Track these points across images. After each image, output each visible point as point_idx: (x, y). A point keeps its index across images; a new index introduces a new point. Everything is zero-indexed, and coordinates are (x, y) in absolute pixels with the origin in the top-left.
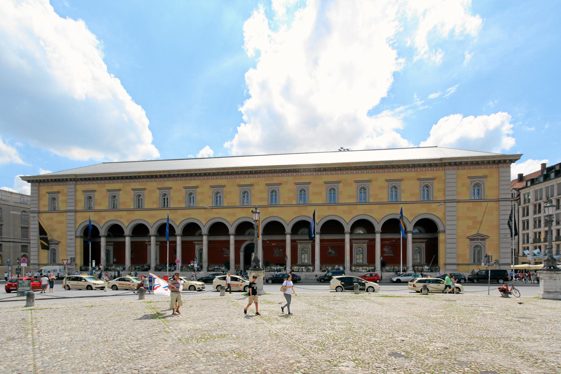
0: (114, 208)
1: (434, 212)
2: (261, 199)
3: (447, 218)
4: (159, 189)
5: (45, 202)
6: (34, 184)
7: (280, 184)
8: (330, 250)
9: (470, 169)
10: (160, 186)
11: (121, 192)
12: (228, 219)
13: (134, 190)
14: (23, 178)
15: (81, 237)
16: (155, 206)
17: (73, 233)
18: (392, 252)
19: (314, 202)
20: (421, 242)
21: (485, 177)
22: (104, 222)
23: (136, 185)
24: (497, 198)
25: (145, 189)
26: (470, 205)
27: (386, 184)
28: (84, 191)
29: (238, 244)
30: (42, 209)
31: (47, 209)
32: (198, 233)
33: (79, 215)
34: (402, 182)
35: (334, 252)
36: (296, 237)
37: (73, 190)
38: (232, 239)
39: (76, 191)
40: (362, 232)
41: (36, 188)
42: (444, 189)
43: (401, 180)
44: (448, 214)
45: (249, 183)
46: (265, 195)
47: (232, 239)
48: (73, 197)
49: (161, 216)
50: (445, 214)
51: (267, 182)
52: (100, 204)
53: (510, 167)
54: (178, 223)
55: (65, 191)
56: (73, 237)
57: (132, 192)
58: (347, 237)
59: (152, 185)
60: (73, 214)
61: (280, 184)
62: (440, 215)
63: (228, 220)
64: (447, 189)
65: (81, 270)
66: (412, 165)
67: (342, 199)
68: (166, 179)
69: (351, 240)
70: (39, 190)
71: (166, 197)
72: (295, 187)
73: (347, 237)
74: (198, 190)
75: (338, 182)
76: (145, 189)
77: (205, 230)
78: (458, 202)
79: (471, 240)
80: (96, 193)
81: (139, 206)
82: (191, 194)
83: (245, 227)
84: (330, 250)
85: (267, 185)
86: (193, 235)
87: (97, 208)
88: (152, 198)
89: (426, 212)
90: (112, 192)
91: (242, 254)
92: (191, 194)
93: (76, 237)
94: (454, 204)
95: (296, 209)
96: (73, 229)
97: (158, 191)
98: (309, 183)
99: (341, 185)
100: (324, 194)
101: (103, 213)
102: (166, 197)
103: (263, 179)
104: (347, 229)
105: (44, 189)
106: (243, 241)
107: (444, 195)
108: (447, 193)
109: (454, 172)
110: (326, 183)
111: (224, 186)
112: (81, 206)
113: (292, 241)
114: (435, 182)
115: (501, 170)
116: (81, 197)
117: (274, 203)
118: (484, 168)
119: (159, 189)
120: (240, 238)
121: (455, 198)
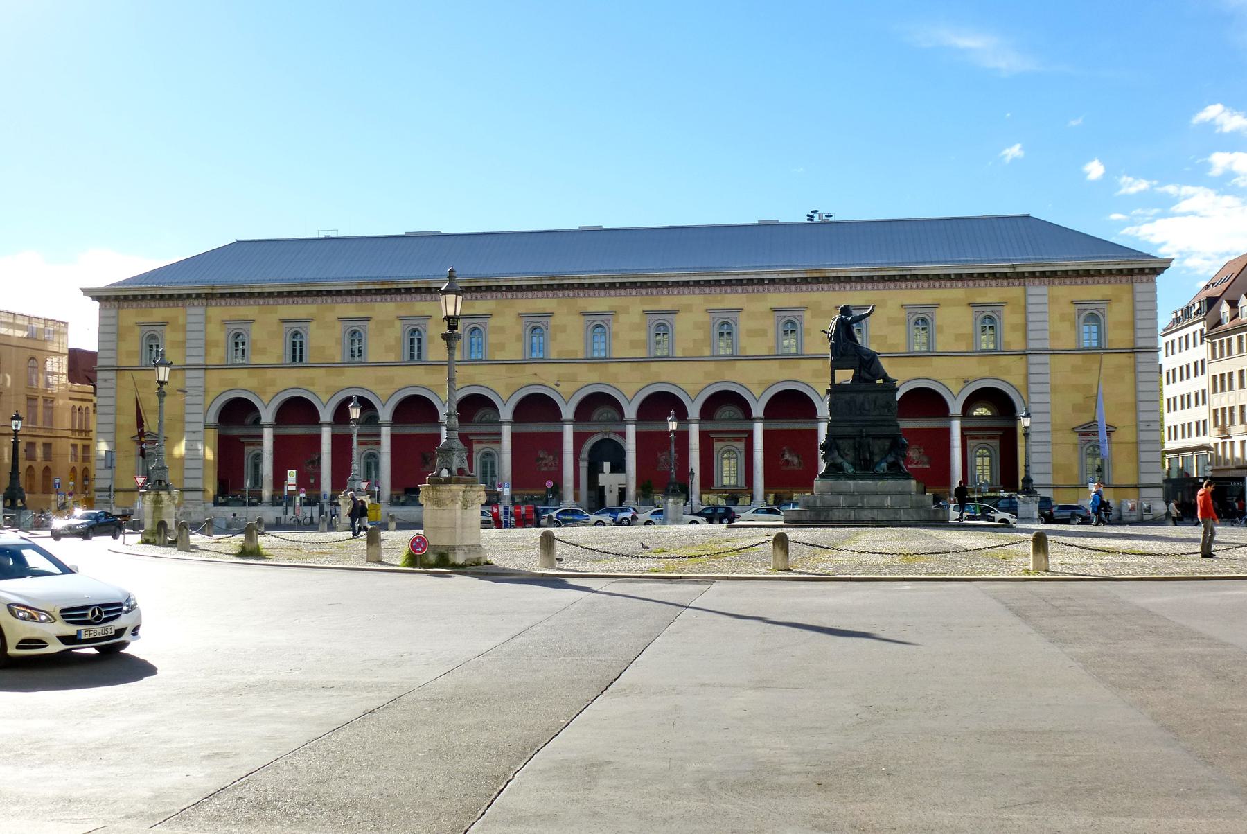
0: (355, 355)
1: (1008, 375)
2: (634, 344)
3: (1033, 388)
4: (401, 318)
5: (134, 343)
6: (108, 305)
7: (674, 312)
8: (787, 456)
9: (812, 290)
10: (403, 313)
11: (313, 325)
12: (565, 388)
13: (342, 320)
14: (86, 292)
15: (215, 427)
16: (392, 358)
17: (200, 418)
18: (925, 459)
19: (750, 352)
20: (990, 438)
21: (1107, 301)
22: (271, 391)
23: (349, 309)
24: (1131, 346)
25: (368, 319)
26: (1077, 360)
27: (903, 314)
28: (225, 322)
29: (579, 439)
30: (125, 362)
31: (135, 362)
32: (249, 420)
33: (214, 376)
34: (676, 317)
35: (796, 460)
36: (709, 427)
37: (201, 319)
38: (568, 432)
39: (207, 320)
40: (989, 413)
41: (113, 313)
42: (1026, 326)
43: (935, 306)
44: (1033, 378)
45: (606, 309)
46: (642, 336)
47: (568, 432)
48: (201, 335)
49: (289, 383)
50: (1027, 377)
51: (647, 308)
52: (263, 351)
53: (1153, 281)
54: (266, 399)
55: (181, 321)
56: (201, 427)
57: (339, 325)
58: (956, 427)
59: (386, 309)
60: (201, 373)
61: (674, 312)
62: (1017, 380)
63: (377, 392)
64: (1031, 326)
65: (216, 504)
66: (956, 275)
67: (372, 355)
68: (418, 297)
69: (963, 430)
70: (117, 317)
71: (240, 340)
72: (707, 318)
73: (956, 427)
74: (491, 322)
75: (802, 309)
76: (368, 319)
77: (267, 416)
78: (1053, 353)
79: (1082, 434)
80: (254, 327)
81: (355, 355)
82: (238, 335)
83: (596, 404)
84: (787, 456)
85: (646, 313)
86: (241, 423)
87: (256, 360)
88: (384, 341)
89: (596, 380)
90: (655, 317)
91: (584, 465)
92: (238, 335)
93: (206, 427)
94: (1046, 359)
95: (710, 366)
96: (200, 409)
97: (398, 324)
98: (739, 310)
99: (807, 315)
100: (771, 333)
101: (270, 373)
102: (416, 337)
103: (638, 298)
104: (956, 408)
105: (131, 315)
106: (592, 434)
107: (1026, 337)
108: (1031, 335)
109: (200, 310)
110: (774, 310)
111: (550, 315)
112: (217, 356)
113: (704, 436)
114: (1006, 310)
115: (1139, 287)
116: (219, 335)
117: (357, 359)
118: (929, 287)
119: (401, 318)
120: (585, 428)
121: (1047, 345)
